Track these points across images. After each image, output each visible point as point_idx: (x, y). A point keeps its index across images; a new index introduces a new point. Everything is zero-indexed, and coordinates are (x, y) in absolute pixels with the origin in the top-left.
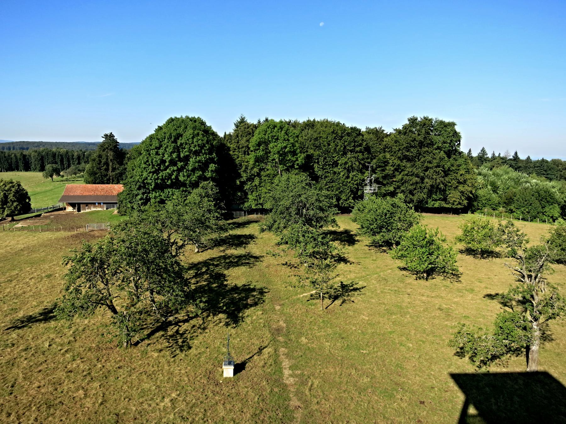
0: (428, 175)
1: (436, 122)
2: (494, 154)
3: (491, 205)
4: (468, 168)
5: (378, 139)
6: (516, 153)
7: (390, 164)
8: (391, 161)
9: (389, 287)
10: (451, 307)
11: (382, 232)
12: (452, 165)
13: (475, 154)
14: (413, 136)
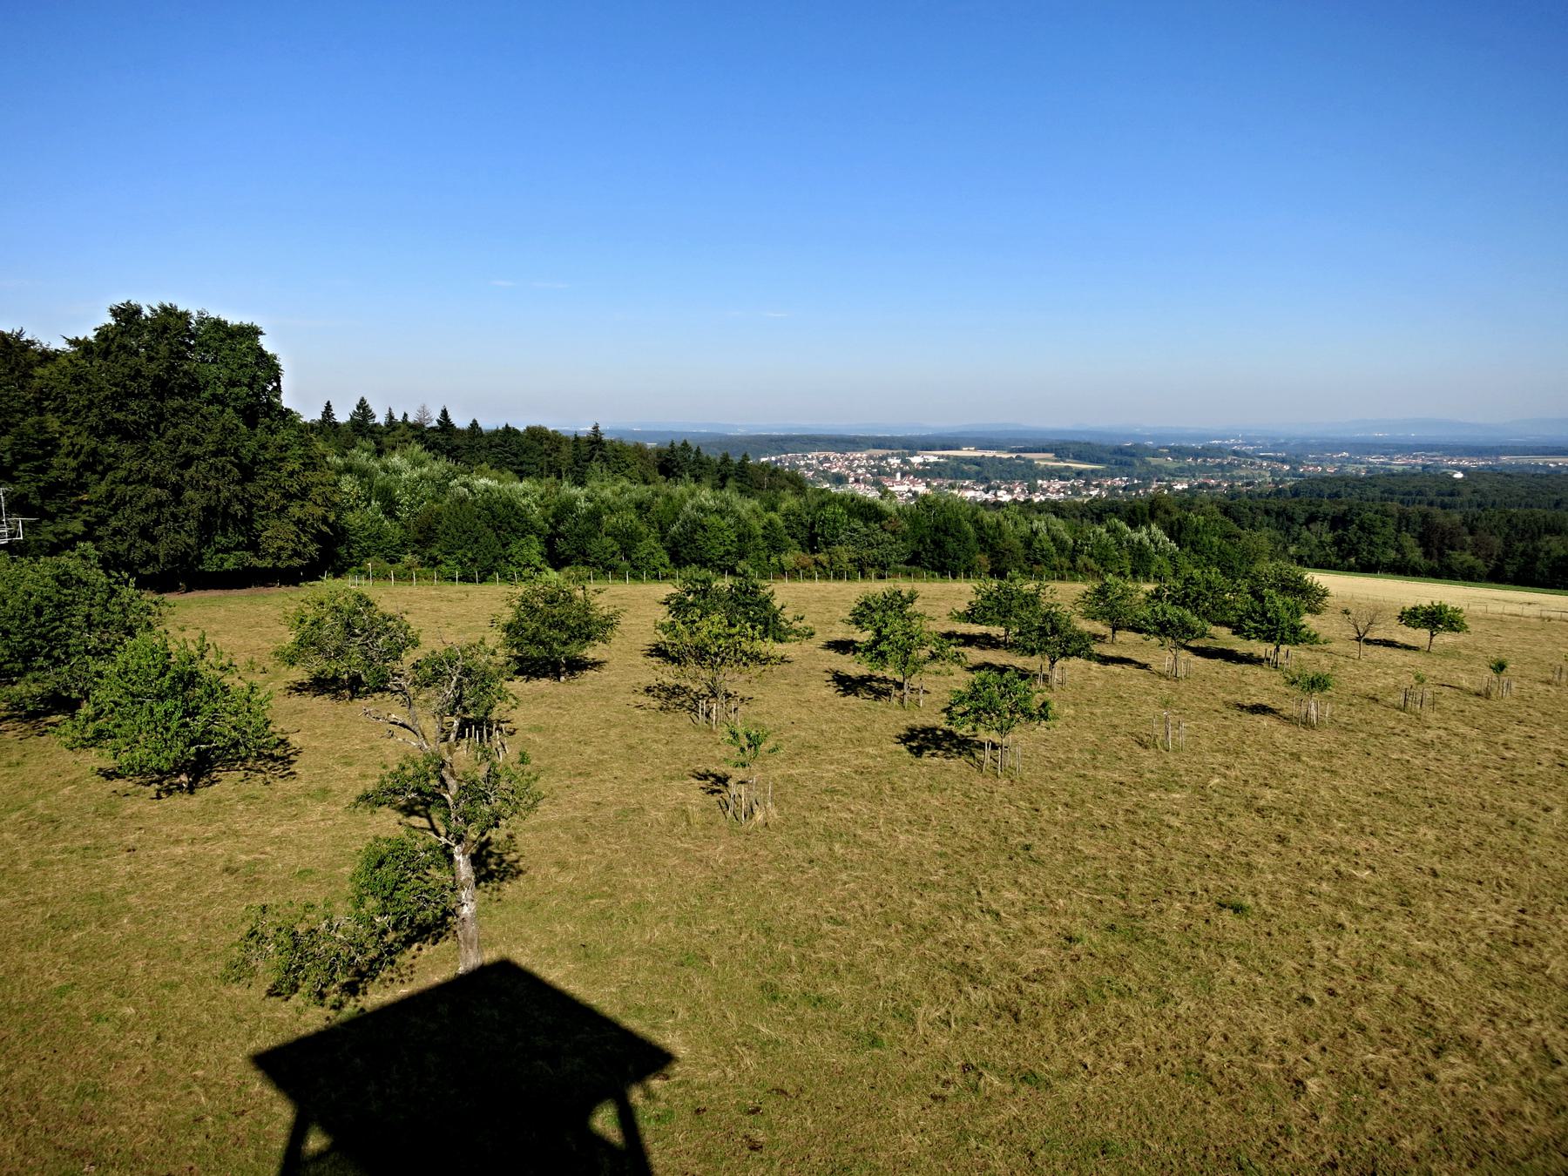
0: (192, 477)
1: (200, 323)
2: (391, 416)
3: (382, 550)
4: (311, 453)
5: (12, 370)
6: (444, 413)
7: (63, 451)
8: (65, 441)
9: (65, 841)
10: (262, 857)
11: (32, 669)
12: (264, 447)
13: (342, 416)
14: (133, 361)
